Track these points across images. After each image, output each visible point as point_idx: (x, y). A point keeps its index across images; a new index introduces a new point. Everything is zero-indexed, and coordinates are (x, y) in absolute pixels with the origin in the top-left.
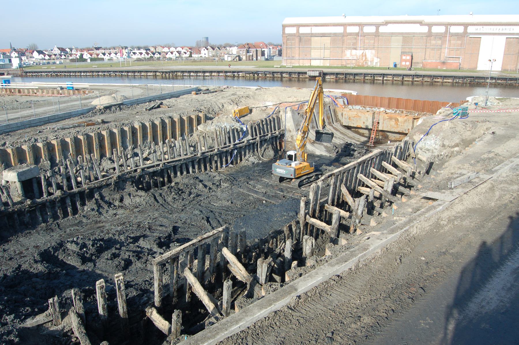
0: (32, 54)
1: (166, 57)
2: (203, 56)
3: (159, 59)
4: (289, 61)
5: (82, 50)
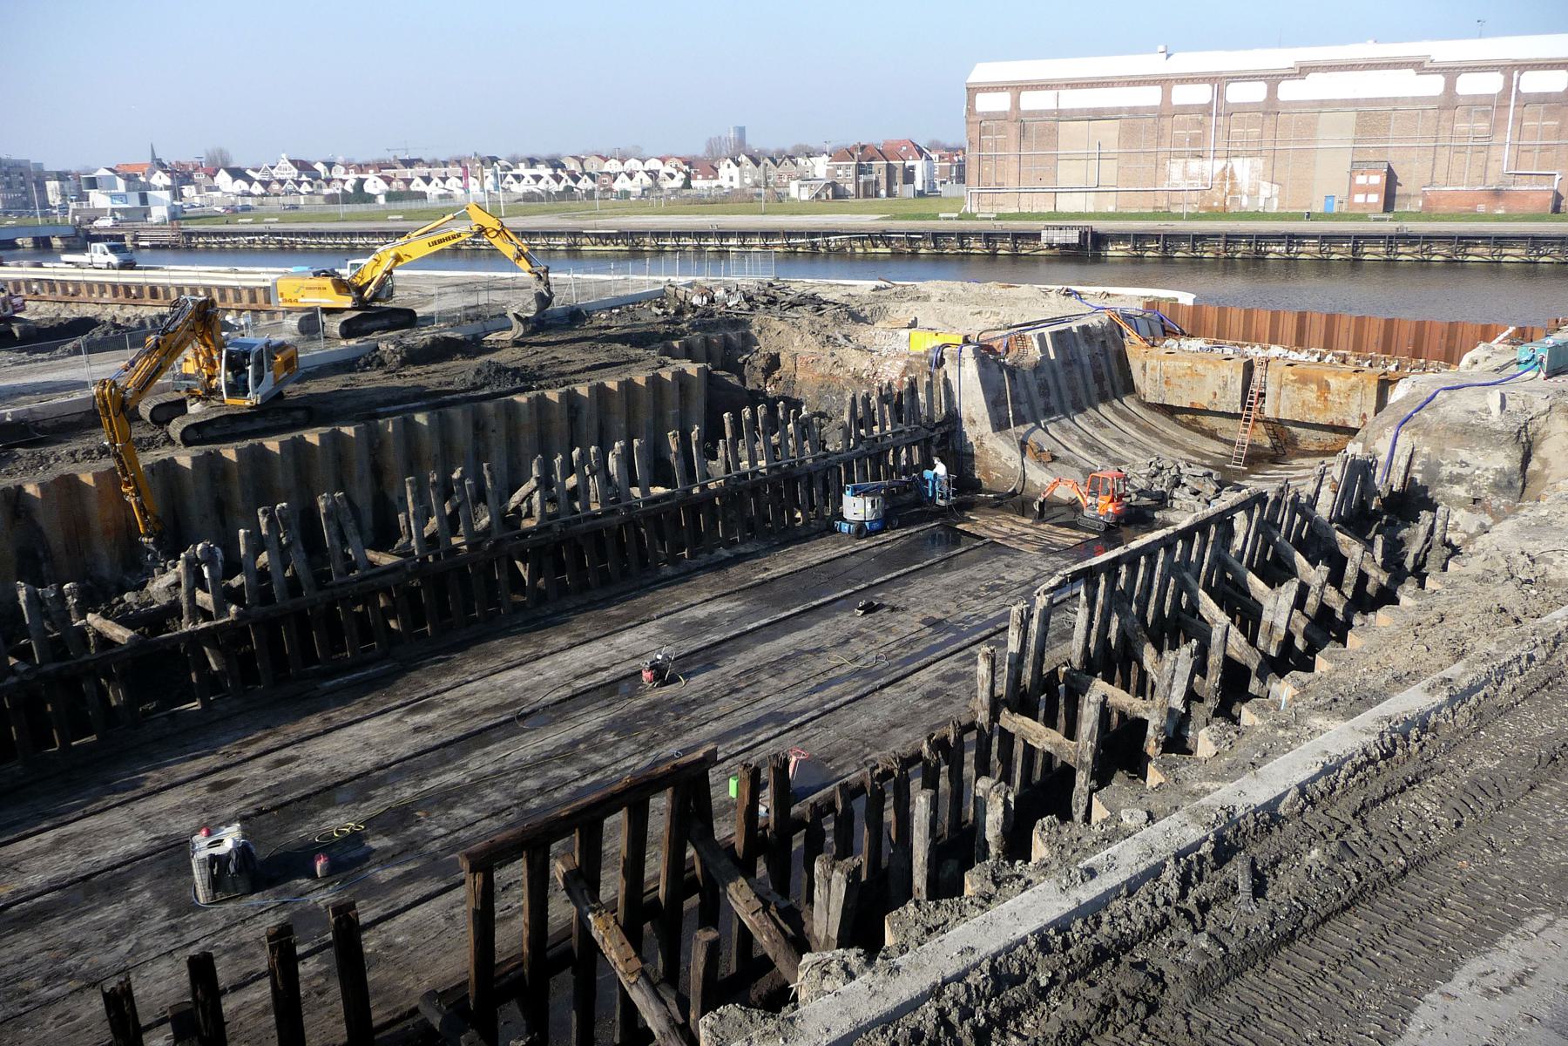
0: (212, 177)
1: (611, 190)
2: (725, 183)
3: (590, 194)
4: (987, 199)
5: (362, 168)
